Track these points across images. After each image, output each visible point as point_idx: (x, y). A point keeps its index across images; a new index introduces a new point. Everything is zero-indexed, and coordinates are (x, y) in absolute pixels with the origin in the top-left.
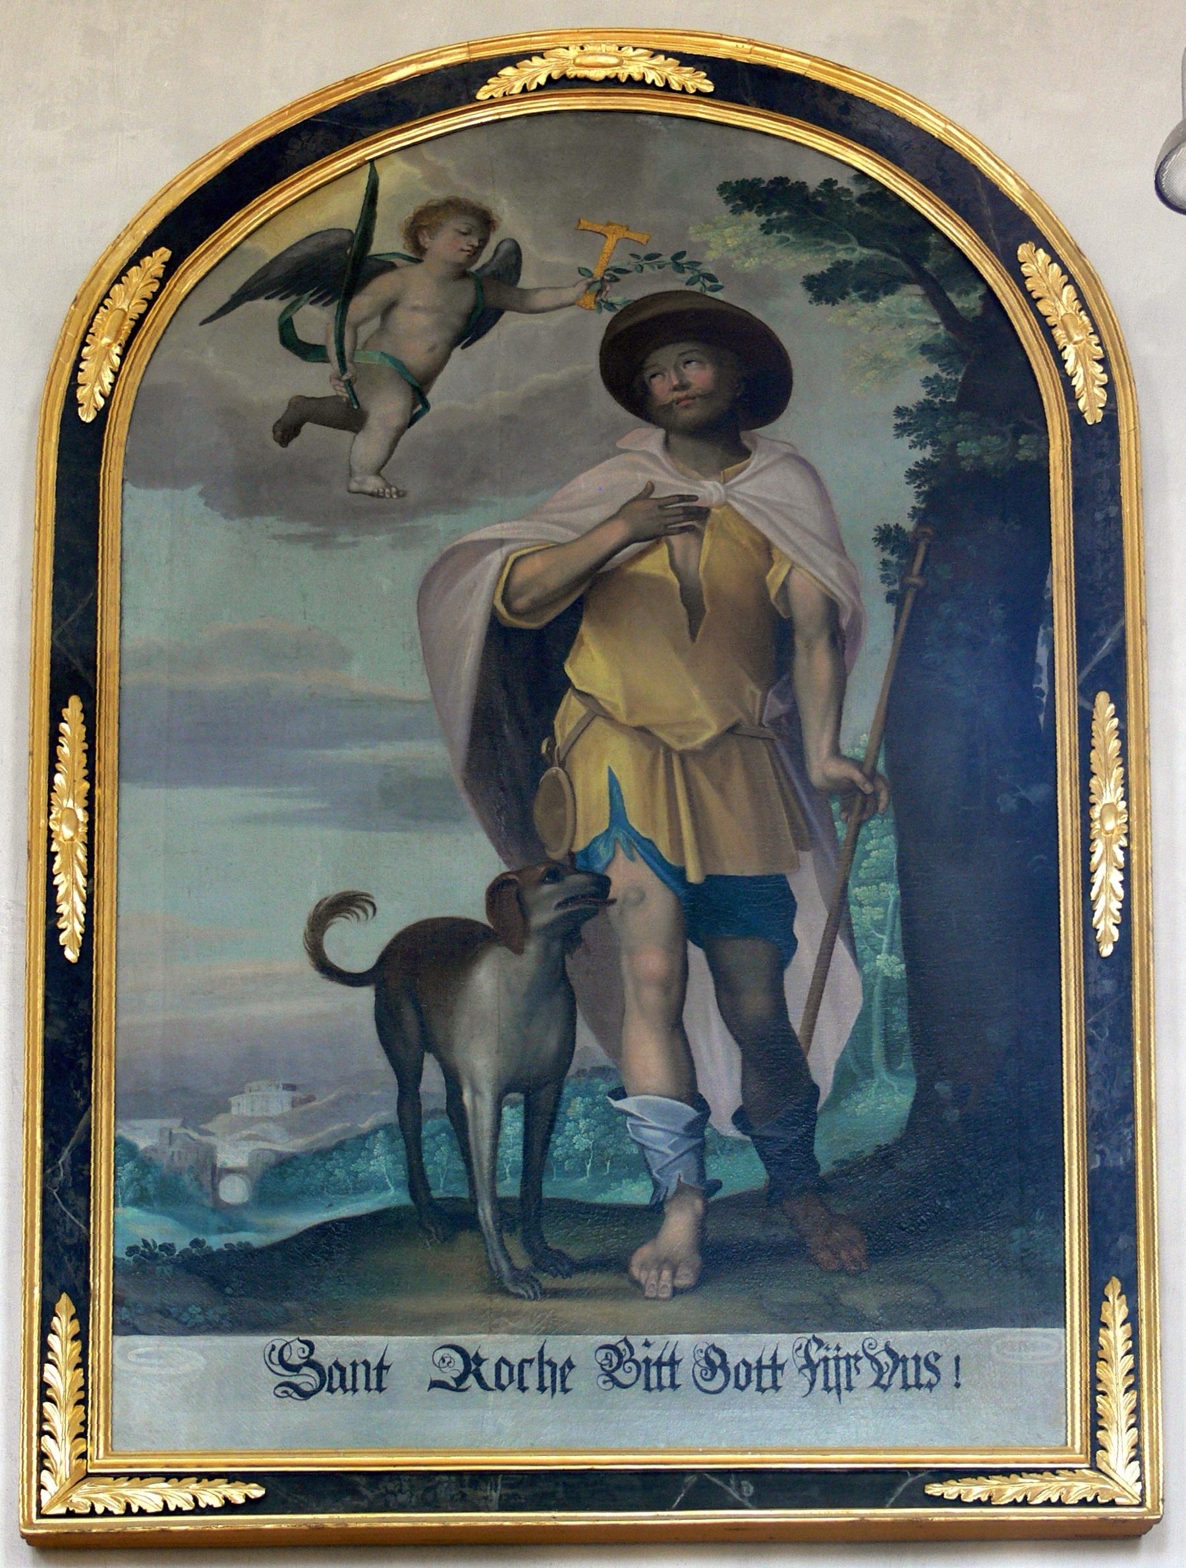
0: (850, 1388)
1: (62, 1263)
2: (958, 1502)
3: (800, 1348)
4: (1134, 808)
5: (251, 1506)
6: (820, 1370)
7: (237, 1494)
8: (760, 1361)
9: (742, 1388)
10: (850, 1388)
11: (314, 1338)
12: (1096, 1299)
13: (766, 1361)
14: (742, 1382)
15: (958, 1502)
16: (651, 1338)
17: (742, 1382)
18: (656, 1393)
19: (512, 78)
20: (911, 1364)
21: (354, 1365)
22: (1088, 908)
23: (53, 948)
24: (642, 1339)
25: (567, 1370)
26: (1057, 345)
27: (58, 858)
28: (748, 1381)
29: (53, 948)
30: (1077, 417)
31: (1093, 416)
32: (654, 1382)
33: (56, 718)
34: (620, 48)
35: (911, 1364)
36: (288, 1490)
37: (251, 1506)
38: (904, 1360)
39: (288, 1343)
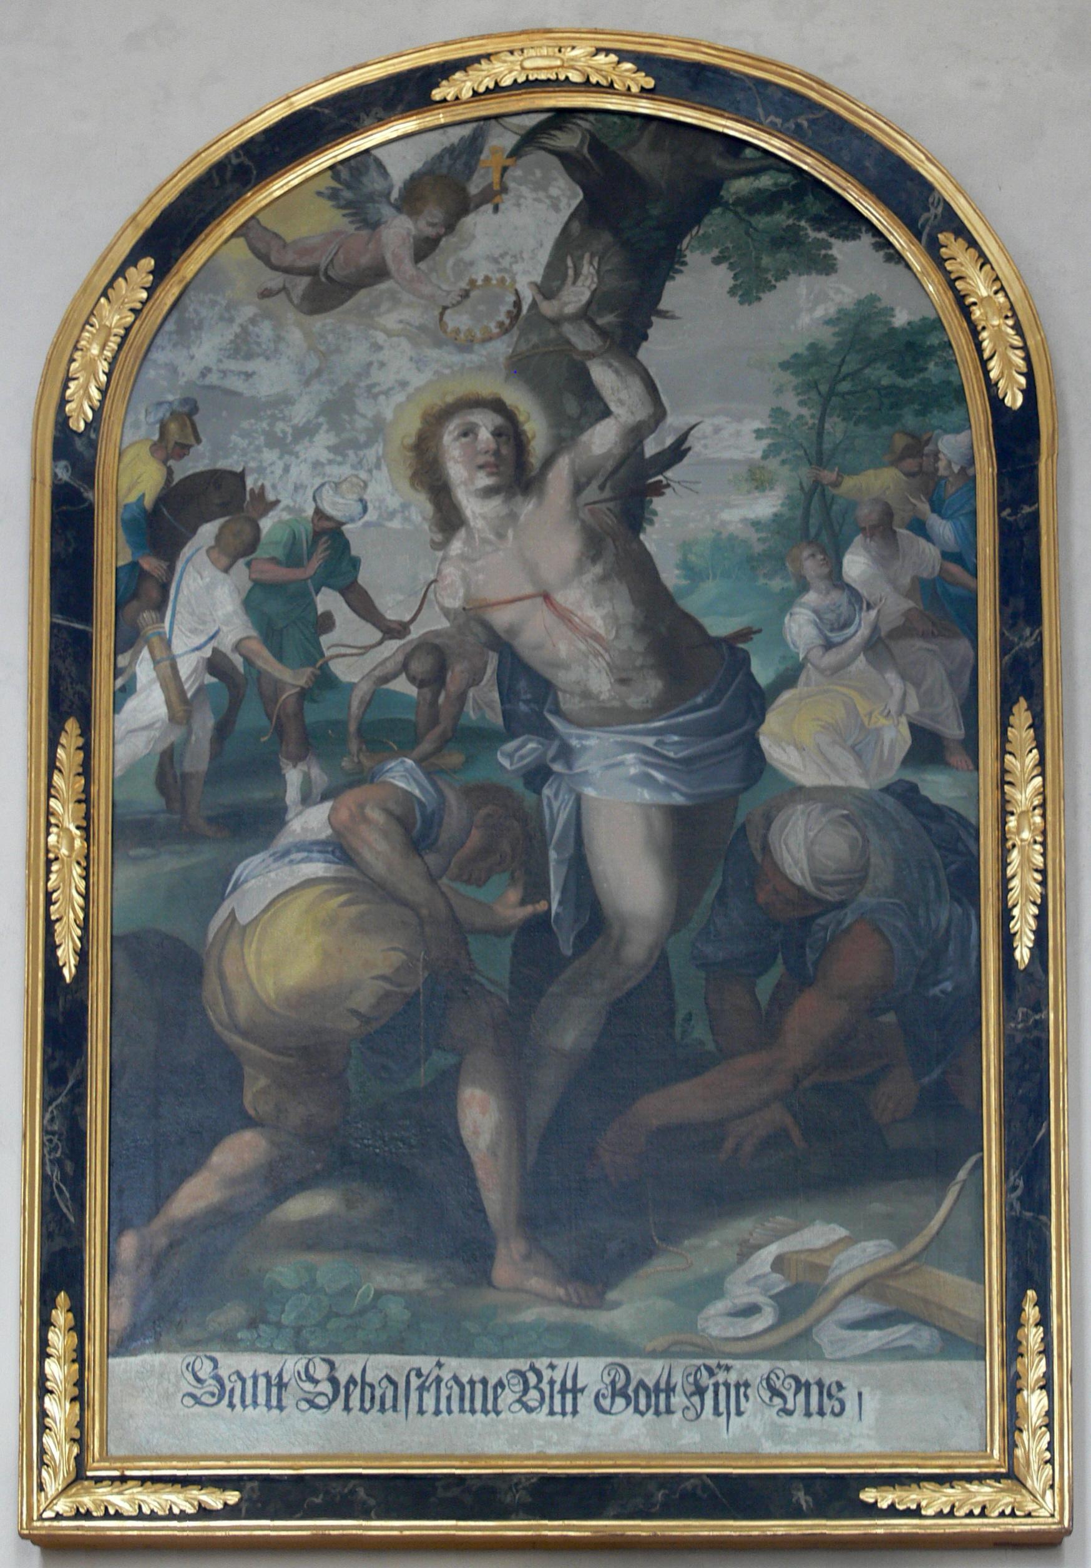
0: (739, 1413)
1: (59, 1272)
2: (892, 1511)
3: (690, 1374)
4: (1049, 818)
5: (229, 1512)
6: (709, 1396)
7: (214, 1500)
8: (658, 1383)
9: (366, 1412)
10: (739, 1413)
11: (337, 1359)
12: (1013, 1320)
13: (663, 1386)
14: (642, 1407)
15: (892, 1511)
16: (555, 1361)
17: (642, 1407)
18: (664, 1417)
19: (461, 85)
20: (815, 1390)
21: (255, 1378)
22: (1005, 916)
23: (53, 969)
24: (546, 1361)
25: (499, 1390)
26: (976, 326)
27: (1045, 1446)
28: (648, 1407)
29: (53, 969)
30: (996, 403)
31: (1014, 400)
32: (557, 1408)
33: (53, 744)
34: (560, 51)
35: (815, 1390)
36: (270, 1494)
37: (229, 1512)
38: (808, 1385)
39: (310, 1360)
